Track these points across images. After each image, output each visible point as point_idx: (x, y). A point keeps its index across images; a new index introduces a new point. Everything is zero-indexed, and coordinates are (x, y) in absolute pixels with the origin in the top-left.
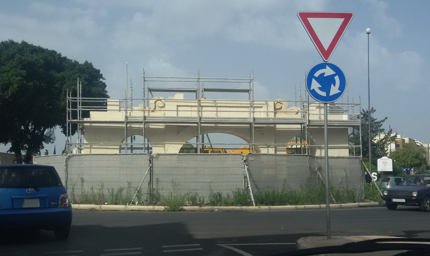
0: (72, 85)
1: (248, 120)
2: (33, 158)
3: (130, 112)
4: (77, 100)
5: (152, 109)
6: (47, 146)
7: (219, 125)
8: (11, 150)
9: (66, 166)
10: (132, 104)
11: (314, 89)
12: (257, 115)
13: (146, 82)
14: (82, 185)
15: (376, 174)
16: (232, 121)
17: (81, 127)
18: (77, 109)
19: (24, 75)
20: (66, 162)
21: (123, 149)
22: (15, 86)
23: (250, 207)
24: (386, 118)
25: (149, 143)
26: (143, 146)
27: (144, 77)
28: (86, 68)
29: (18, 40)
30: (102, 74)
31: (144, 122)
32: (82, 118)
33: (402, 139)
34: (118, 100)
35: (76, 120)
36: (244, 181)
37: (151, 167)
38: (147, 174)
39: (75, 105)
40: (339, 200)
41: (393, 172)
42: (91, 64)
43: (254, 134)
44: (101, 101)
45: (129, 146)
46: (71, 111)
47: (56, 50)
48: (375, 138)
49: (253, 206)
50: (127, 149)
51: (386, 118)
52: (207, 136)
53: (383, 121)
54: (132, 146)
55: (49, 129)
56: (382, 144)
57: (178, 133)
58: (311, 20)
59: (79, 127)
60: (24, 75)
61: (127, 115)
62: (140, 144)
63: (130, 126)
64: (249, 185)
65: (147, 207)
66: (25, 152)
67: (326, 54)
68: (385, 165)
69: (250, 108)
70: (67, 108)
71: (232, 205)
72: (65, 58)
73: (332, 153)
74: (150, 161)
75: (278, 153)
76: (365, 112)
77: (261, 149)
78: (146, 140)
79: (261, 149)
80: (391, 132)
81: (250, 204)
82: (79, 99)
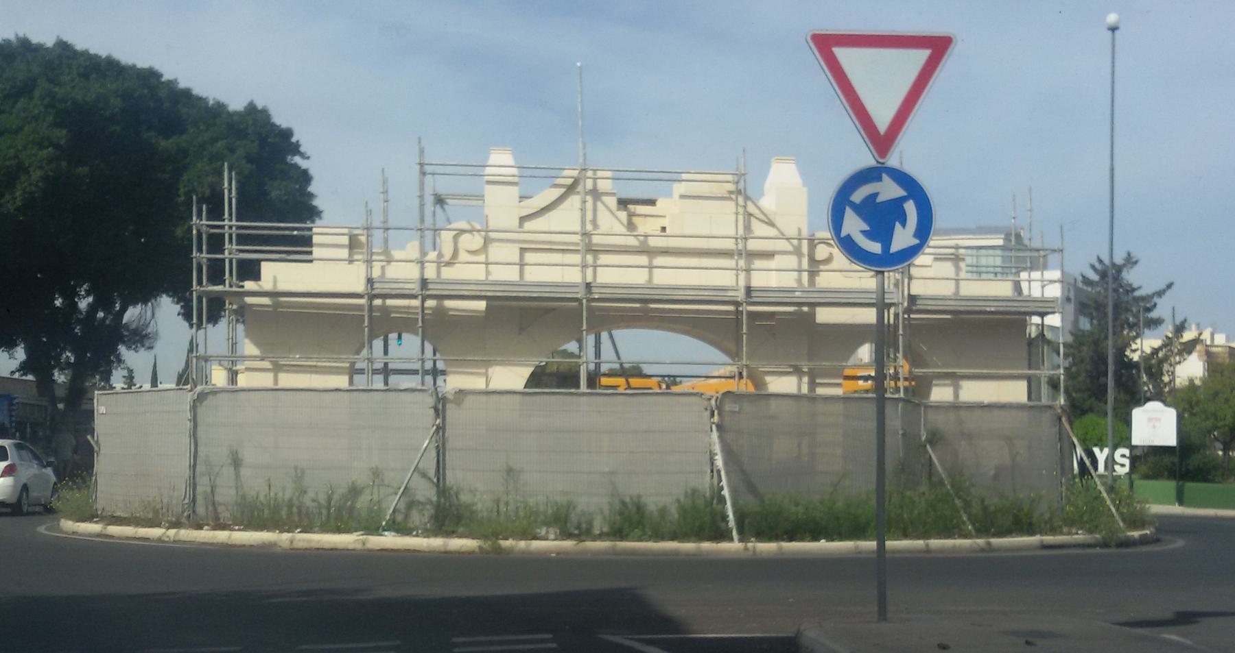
0: (207, 176)
1: (730, 293)
2: (96, 395)
3: (383, 268)
4: (222, 227)
5: (447, 256)
6: (133, 358)
7: (652, 306)
8: (24, 368)
9: (192, 422)
10: (386, 241)
11: (849, 235)
12: (758, 280)
13: (428, 178)
14: (238, 476)
15: (1127, 452)
16: (680, 294)
17: (235, 307)
18: (224, 254)
19: (63, 142)
20: (194, 408)
21: (361, 371)
22: (36, 175)
23: (724, 546)
24: (1170, 286)
25: (438, 356)
26: (417, 366)
27: (420, 164)
28: (251, 122)
29: (44, 36)
30: (298, 141)
31: (420, 297)
32: (237, 279)
33: (1228, 348)
34: (345, 231)
35: (219, 288)
36: (709, 471)
37: (438, 428)
38: (426, 447)
39: (216, 243)
40: (986, 526)
41: (1178, 450)
42: (265, 113)
43: (745, 334)
44: (295, 233)
45: (379, 365)
46: (205, 260)
47: (159, 66)
48: (1134, 347)
49: (731, 539)
50: (370, 372)
51: (1170, 286)
52: (611, 337)
53: (1160, 294)
54: (386, 364)
55: (139, 307)
56: (1155, 366)
57: (522, 329)
58: (841, 53)
59: (230, 307)
60: (63, 142)
61: (371, 274)
62: (409, 360)
63: (384, 303)
64: (724, 483)
65: (426, 540)
66: (66, 375)
67: (882, 142)
68: (1154, 427)
69: (736, 257)
70: (194, 252)
71: (673, 537)
72: (187, 93)
73: (975, 391)
74: (436, 410)
75: (820, 391)
76: (1104, 264)
77: (768, 379)
78: (429, 348)
79: (768, 379)
80: (1180, 329)
81: (724, 536)
82: (230, 224)
